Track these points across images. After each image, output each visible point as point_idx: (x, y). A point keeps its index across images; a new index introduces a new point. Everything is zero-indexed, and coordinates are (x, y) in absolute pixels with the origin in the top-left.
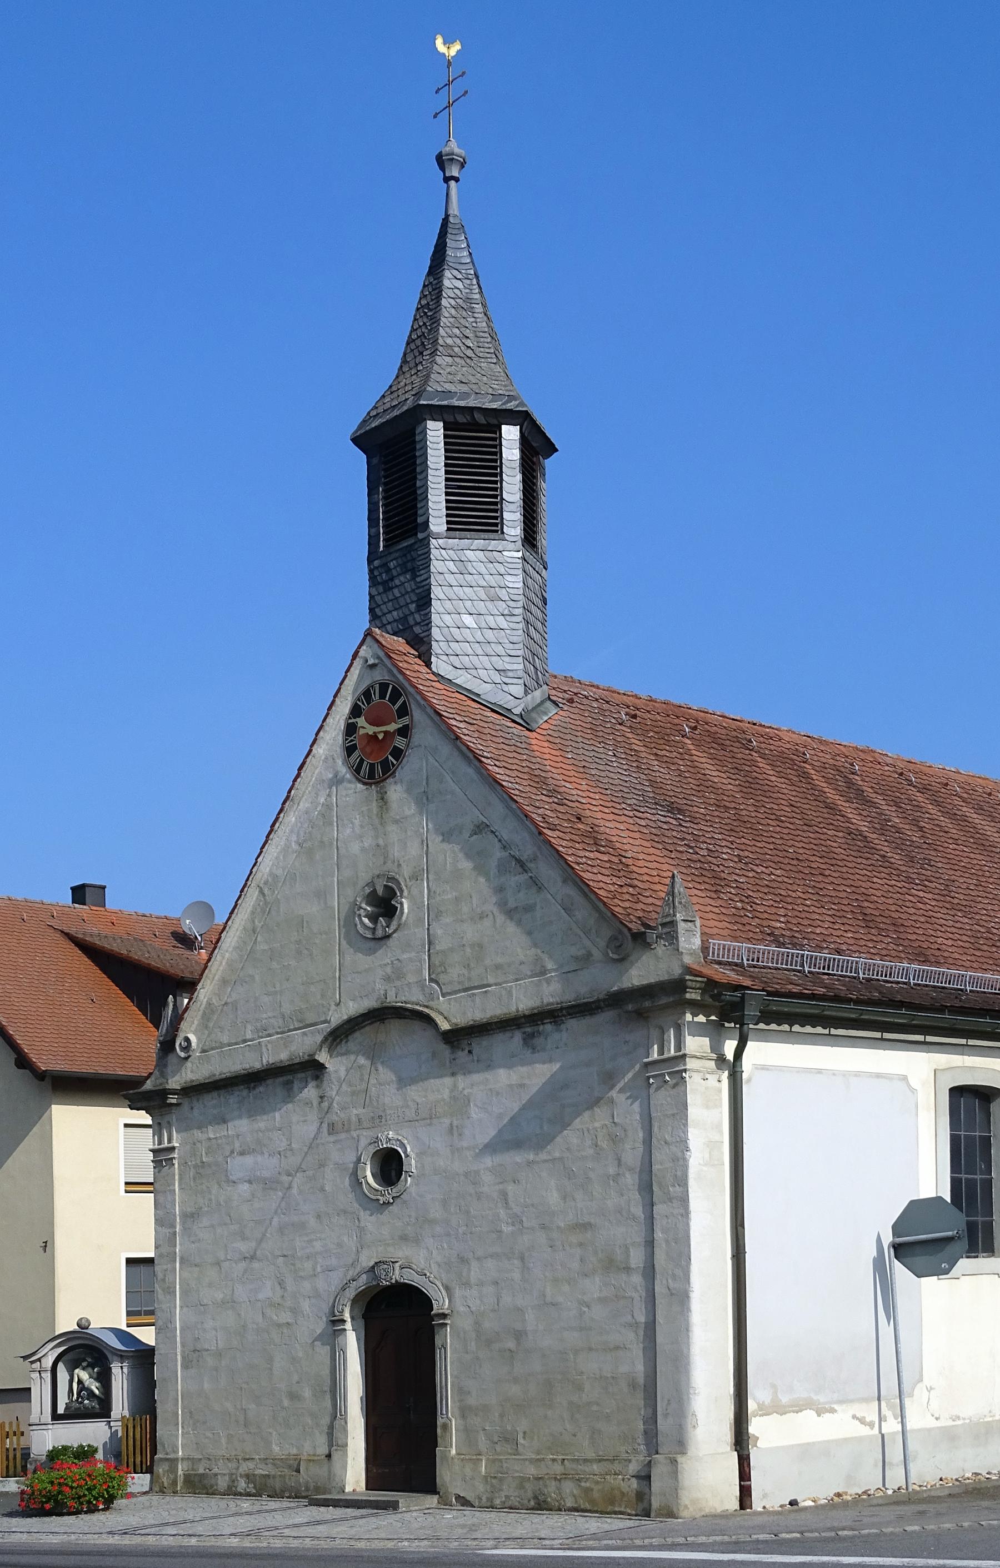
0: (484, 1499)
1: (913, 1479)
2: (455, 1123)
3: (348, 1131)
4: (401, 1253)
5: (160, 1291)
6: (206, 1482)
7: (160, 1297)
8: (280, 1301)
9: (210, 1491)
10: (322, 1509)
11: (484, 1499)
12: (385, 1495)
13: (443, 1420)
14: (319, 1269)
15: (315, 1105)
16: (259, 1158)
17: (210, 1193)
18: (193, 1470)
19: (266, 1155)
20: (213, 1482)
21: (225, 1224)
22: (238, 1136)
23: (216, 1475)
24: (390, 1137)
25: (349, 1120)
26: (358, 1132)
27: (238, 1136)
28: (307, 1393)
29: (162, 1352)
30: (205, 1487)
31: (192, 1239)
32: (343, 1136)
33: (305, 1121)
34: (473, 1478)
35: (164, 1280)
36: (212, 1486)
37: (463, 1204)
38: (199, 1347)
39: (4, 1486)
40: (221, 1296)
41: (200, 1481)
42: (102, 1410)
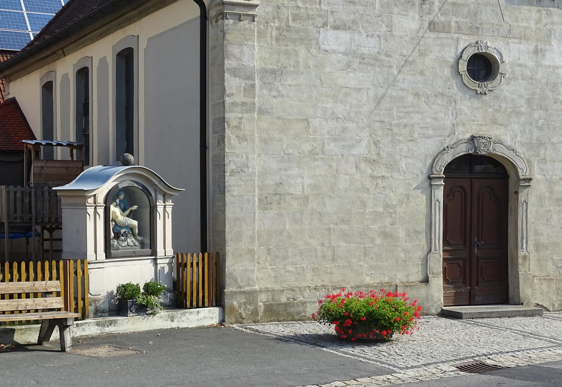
0: (556, 306)
1: (90, 271)
2: (539, 47)
3: (449, 32)
4: (494, 132)
5: (233, 137)
6: (292, 310)
7: (233, 142)
8: (374, 157)
9: (298, 317)
10: (490, 319)
11: (556, 306)
12: (490, 308)
13: (524, 253)
14: (416, 135)
15: (417, 4)
16: (356, 36)
17: (297, 56)
18: (273, 299)
19: (364, 35)
20: (301, 309)
21: (315, 86)
22: (332, 12)
23: (304, 303)
24: (493, 46)
25: (449, 23)
26: (457, 35)
27: (332, 12)
28: (402, 233)
29: (235, 193)
30: (290, 314)
31: (274, 93)
32: (443, 35)
33: (406, 15)
34: (548, 292)
35: (238, 127)
36: (299, 313)
37: (543, 104)
38: (280, 190)
39: (84, 330)
40: (309, 148)
41: (285, 310)
42: (149, 246)
